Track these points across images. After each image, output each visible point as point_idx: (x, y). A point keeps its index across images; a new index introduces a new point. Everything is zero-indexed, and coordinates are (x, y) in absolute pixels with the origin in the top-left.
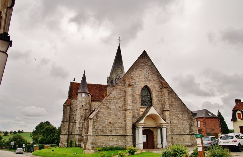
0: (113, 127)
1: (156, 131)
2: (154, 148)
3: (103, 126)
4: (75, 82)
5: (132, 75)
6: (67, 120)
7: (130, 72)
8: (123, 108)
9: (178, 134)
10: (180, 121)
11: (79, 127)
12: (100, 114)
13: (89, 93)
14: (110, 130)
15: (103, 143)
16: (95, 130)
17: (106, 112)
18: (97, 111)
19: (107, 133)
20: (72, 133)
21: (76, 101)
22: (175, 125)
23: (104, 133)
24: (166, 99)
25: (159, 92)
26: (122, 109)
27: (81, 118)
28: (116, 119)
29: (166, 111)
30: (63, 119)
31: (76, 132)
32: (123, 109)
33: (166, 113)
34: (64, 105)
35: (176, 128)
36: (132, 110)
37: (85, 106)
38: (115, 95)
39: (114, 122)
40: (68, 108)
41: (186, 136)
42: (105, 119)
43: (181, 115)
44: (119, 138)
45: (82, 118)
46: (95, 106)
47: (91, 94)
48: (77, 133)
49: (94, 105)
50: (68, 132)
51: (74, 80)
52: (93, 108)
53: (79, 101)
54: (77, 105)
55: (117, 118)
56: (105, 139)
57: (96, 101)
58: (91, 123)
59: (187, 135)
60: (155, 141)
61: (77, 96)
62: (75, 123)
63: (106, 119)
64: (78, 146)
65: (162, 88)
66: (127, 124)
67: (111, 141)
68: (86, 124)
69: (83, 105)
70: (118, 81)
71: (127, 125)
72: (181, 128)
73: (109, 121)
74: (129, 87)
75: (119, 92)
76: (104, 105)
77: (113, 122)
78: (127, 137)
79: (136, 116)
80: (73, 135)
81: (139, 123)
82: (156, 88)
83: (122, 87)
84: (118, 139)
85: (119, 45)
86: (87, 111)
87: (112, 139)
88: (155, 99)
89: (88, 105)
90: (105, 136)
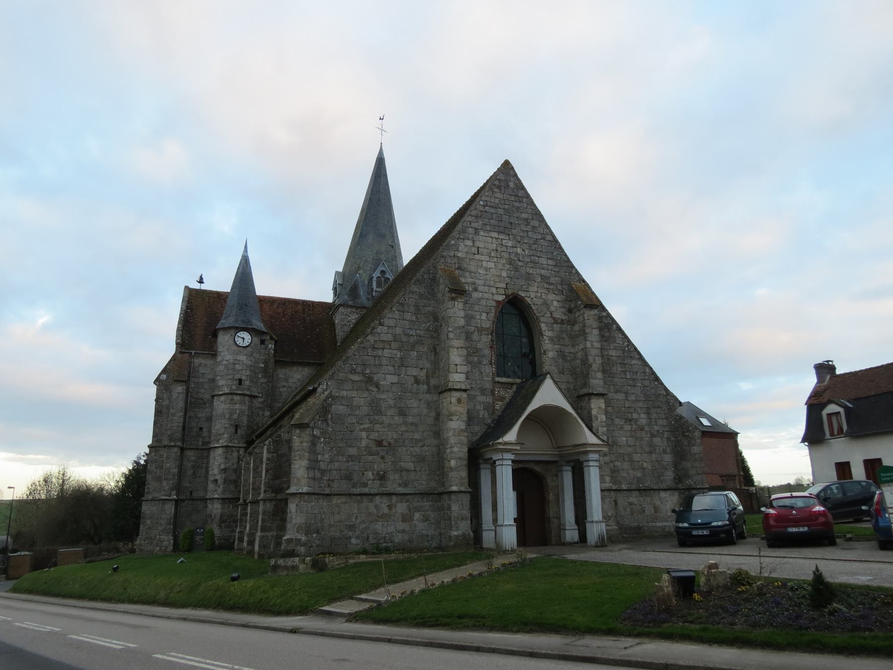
0: (389, 459)
1: (556, 475)
2: (546, 545)
3: (351, 458)
4: (204, 287)
5: (460, 255)
6: (171, 440)
7: (453, 242)
8: (428, 384)
9: (634, 487)
10: (642, 439)
11: (223, 467)
12: (339, 409)
13: (264, 329)
14: (378, 474)
15: (352, 527)
16: (318, 474)
17: (361, 399)
18: (326, 393)
19: (366, 485)
20: (191, 492)
21: (209, 362)
22: (622, 451)
23: (354, 486)
24: (594, 352)
25: (562, 322)
26: (425, 387)
27: (232, 430)
28: (403, 428)
29: (593, 397)
30: (154, 437)
31: (211, 486)
32: (429, 388)
33: (592, 406)
34: (158, 381)
35: (626, 465)
36: (465, 391)
37: (251, 381)
38: (398, 331)
39: (396, 441)
40: (180, 389)
41: (663, 494)
42: (358, 428)
43: (643, 416)
44: (415, 504)
45: (236, 432)
46: (287, 382)
47: (274, 336)
48: (216, 490)
49: (287, 380)
50: (178, 488)
51: (201, 278)
52: (283, 390)
53: (225, 362)
54: (213, 380)
55: (405, 423)
56: (358, 510)
57: (294, 364)
58: (299, 441)
59: (668, 492)
60: (551, 513)
61: (216, 342)
62: (205, 454)
63: (362, 427)
64: (220, 548)
65: (576, 307)
66: (445, 450)
67: (383, 516)
68: (269, 452)
69: (240, 381)
70: (378, 289)
71: (448, 451)
72: (645, 465)
73: (374, 436)
74: (453, 299)
75: (414, 318)
76: (353, 371)
77: (392, 441)
78: (450, 500)
79: (481, 416)
80: (199, 502)
81: (500, 440)
82: (552, 308)
83: (425, 301)
84: (410, 510)
85: (246, 247)
86: (257, 403)
87: (386, 510)
88: (549, 350)
89: (262, 380)
90: (359, 498)
